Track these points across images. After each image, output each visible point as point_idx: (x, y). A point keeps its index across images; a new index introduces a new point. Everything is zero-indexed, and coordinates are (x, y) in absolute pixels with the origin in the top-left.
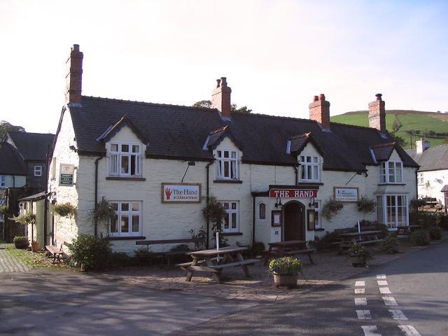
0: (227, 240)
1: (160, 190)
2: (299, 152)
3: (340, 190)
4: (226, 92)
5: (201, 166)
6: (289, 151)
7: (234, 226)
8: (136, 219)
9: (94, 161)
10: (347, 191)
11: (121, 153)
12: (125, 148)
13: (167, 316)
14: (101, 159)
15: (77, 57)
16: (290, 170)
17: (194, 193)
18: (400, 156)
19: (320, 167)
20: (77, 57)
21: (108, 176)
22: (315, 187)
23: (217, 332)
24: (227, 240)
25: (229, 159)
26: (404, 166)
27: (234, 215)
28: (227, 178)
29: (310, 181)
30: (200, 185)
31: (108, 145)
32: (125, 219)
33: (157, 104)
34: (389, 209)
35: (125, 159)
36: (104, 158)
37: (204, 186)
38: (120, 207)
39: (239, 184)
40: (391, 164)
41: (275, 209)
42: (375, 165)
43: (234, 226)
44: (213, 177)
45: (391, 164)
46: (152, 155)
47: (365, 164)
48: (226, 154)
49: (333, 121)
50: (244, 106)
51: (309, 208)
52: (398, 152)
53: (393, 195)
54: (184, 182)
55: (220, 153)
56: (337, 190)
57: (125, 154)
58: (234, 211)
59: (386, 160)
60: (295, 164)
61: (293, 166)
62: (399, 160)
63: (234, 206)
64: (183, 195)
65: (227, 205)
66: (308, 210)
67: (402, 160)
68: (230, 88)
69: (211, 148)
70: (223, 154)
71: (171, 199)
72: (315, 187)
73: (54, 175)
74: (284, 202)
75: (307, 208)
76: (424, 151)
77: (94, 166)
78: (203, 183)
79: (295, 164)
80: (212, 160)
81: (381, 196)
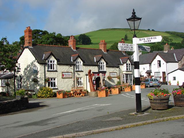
0: (144, 85)
2: (99, 61)
3: (111, 73)
5: (72, 67)
6: (95, 61)
10: (113, 73)
17: (70, 75)
18: (130, 61)
21: (83, 72)
22: (104, 73)
24: (144, 85)
28: (51, 70)
29: (102, 70)
32: (52, 83)
35: (51, 65)
41: (94, 79)
43: (81, 85)
44: (46, 69)
48: (51, 62)
49: (33, 30)
52: (129, 60)
58: (81, 80)
62: (130, 63)
63: (54, 79)
64: (67, 76)
66: (93, 80)
67: (131, 63)
71: (64, 77)
72: (104, 73)
74: (96, 77)
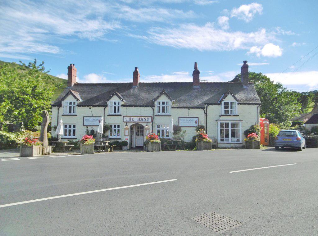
1: (83, 119)
7: (74, 135)
8: (74, 131)
11: (161, 105)
12: (163, 103)
15: (196, 64)
16: (149, 109)
20: (196, 64)
21: (108, 114)
25: (165, 105)
30: (151, 116)
31: (109, 103)
33: (189, 82)
34: (221, 130)
36: (107, 108)
38: (113, 126)
39: (120, 116)
46: (128, 106)
48: (115, 103)
50: (255, 72)
53: (227, 122)
56: (197, 119)
57: (115, 105)
61: (150, 106)
65: (111, 126)
70: (161, 103)
73: (47, 114)
78: (152, 116)
81: (237, 125)
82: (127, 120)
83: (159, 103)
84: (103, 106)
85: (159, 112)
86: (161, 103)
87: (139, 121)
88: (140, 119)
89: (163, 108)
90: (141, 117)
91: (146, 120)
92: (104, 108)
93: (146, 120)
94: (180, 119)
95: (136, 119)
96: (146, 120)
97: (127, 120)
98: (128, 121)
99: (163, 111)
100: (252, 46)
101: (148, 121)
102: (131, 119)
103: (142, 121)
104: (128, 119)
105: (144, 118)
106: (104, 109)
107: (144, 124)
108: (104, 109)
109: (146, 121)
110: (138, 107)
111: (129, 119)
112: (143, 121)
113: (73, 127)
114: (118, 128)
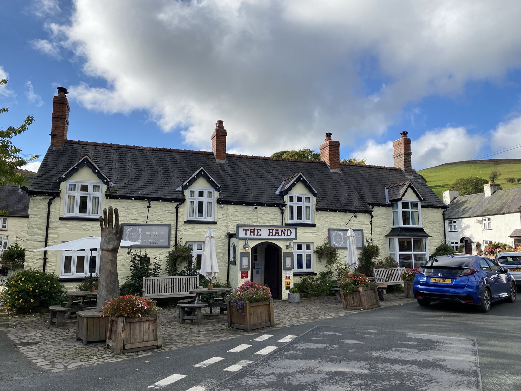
4: (334, 147)
9: (48, 201)
12: (84, 188)
13: (146, 353)
14: (54, 198)
16: (275, 210)
19: (313, 208)
23: (496, 327)
26: (422, 206)
27: (199, 257)
31: (64, 186)
36: (57, 199)
37: (173, 228)
40: (405, 205)
42: (386, 205)
44: (55, 214)
45: (405, 205)
47: (374, 205)
48: (201, 194)
51: (286, 251)
54: (149, 223)
55: (291, 199)
59: (399, 200)
60: (281, 206)
61: (278, 205)
66: (241, 253)
68: (225, 131)
69: (283, 194)
70: (295, 199)
75: (284, 250)
76: (492, 194)
77: (47, 205)
78: (173, 222)
79: (281, 206)
80: (182, 201)
82: (246, 235)
83: (291, 199)
84: (176, 200)
85: (292, 218)
86: (295, 199)
87: (271, 237)
88: (274, 232)
89: (300, 209)
90: (275, 229)
91: (284, 234)
92: (175, 204)
93: (284, 234)
94: (334, 233)
95: (264, 234)
96: (286, 234)
97: (246, 235)
98: (248, 236)
99: (300, 216)
100: (43, 38)
101: (288, 237)
102: (254, 232)
103: (277, 237)
104: (248, 233)
105: (282, 231)
106: (177, 208)
107: (282, 245)
108: (177, 208)
109: (286, 237)
110: (159, 200)
111: (251, 232)
112: (280, 237)
113: (83, 257)
114: (454, 243)
